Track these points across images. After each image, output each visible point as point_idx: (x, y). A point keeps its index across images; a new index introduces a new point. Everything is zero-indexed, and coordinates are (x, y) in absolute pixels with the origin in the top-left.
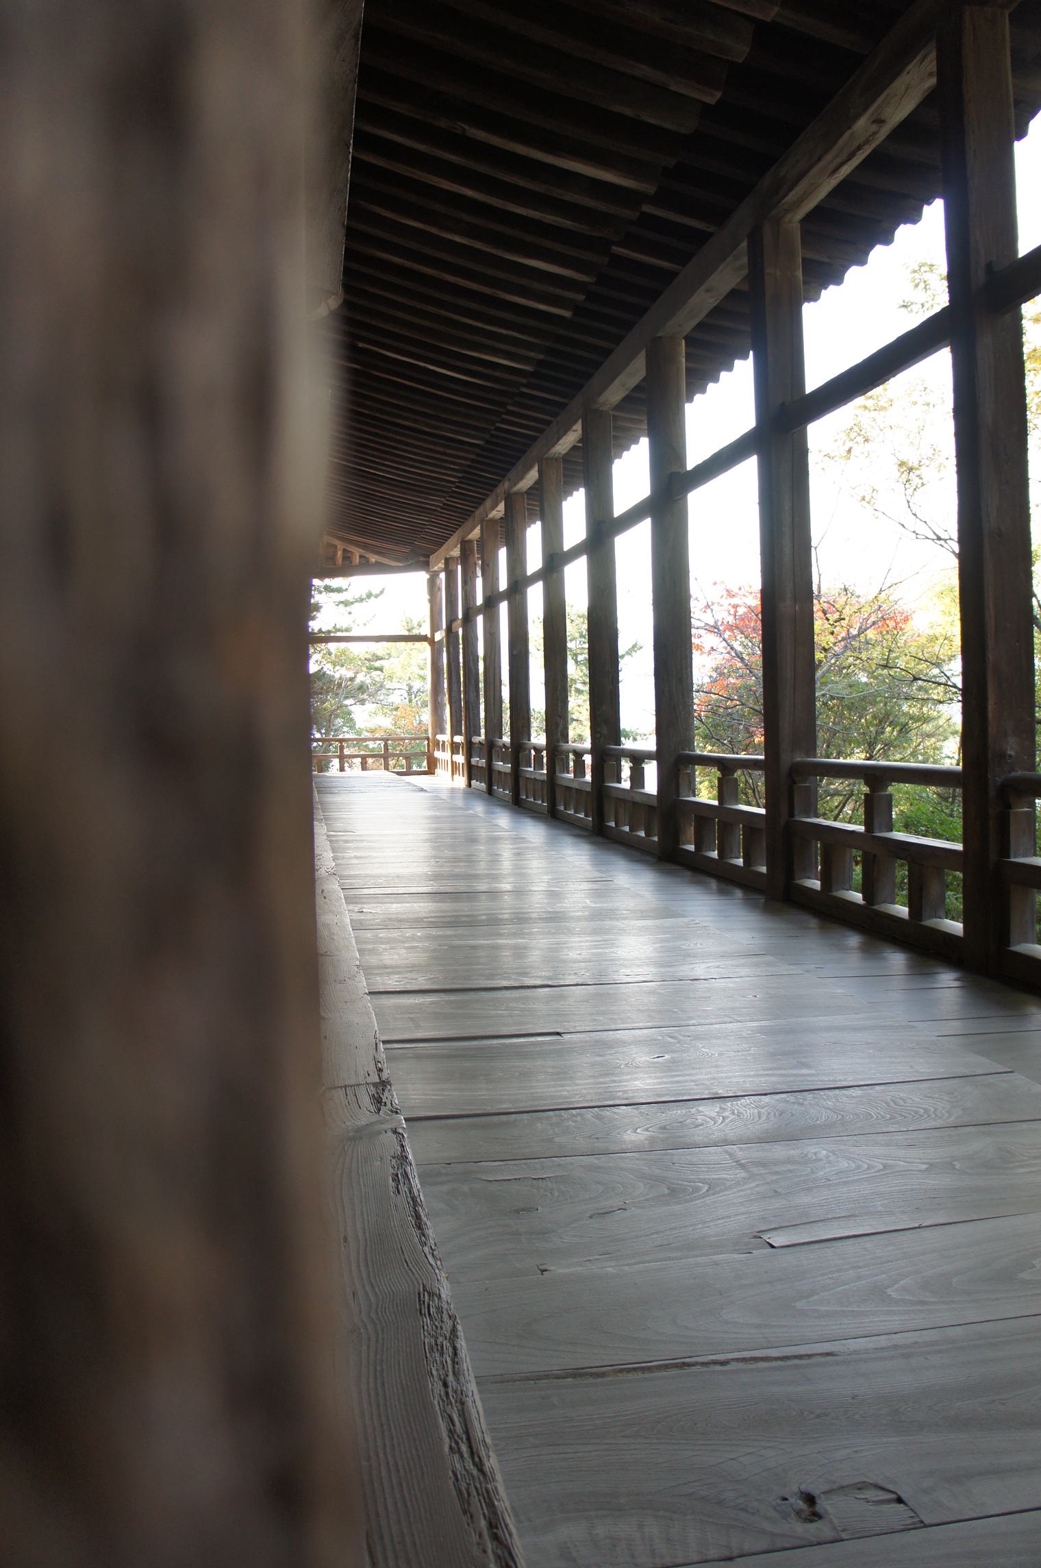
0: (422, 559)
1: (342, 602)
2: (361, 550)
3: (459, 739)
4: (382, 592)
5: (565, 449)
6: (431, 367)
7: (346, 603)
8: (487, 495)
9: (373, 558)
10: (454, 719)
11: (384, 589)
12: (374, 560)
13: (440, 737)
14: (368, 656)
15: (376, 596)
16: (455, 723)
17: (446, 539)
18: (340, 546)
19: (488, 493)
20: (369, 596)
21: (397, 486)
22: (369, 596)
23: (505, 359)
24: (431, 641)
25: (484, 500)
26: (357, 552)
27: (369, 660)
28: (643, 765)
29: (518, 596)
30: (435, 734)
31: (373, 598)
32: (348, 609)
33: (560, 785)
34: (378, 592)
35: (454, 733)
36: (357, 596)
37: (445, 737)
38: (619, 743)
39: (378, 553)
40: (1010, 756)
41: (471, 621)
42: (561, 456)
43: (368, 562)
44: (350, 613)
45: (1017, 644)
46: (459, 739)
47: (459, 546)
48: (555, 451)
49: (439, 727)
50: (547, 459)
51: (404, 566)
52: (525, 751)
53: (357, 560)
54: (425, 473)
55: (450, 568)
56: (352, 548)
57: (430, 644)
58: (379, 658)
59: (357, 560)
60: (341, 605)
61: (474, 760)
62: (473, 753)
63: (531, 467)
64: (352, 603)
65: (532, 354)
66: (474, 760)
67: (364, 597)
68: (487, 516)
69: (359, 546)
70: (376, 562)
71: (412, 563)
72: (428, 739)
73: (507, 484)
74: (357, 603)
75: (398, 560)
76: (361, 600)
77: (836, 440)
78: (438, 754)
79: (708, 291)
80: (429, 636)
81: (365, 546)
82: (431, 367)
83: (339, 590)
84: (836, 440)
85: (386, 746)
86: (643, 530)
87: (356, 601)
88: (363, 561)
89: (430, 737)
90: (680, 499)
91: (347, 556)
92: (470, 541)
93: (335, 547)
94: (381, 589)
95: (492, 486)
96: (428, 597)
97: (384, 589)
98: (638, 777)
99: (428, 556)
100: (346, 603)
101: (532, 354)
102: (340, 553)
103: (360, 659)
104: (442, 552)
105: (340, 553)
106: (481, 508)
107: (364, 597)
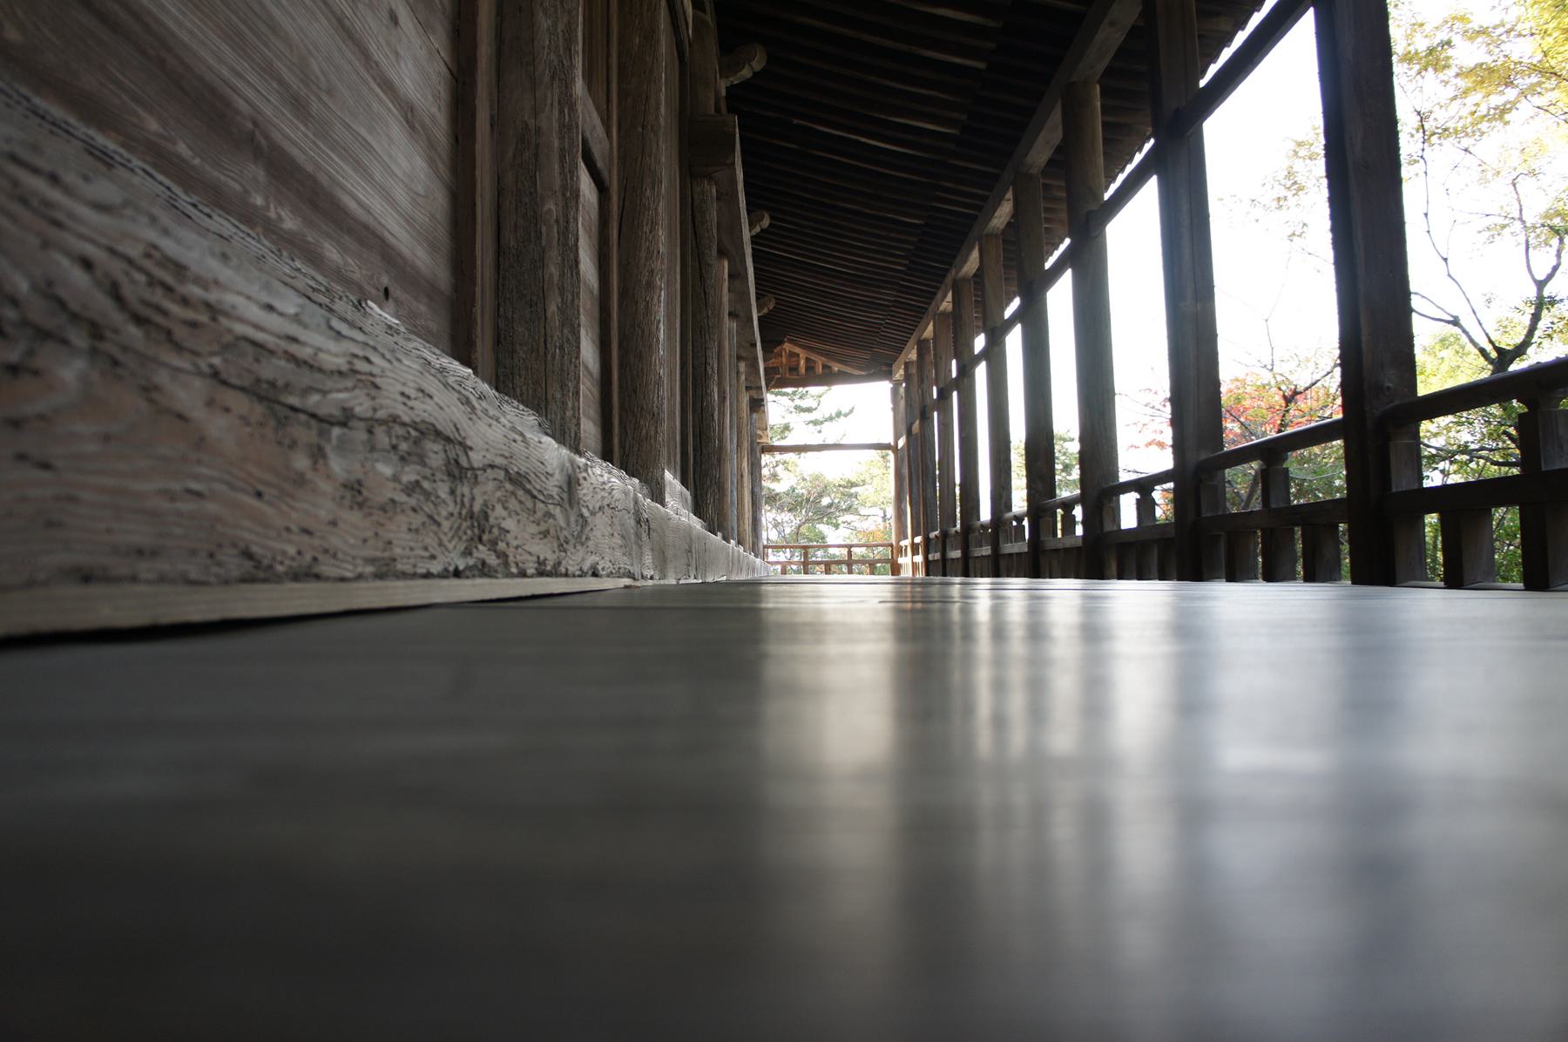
0: (884, 368)
1: (812, 422)
2: (823, 359)
3: (918, 540)
4: (851, 411)
5: (1002, 223)
6: (863, 140)
7: (815, 423)
8: (938, 288)
9: (836, 367)
10: (915, 521)
11: (853, 408)
12: (836, 369)
13: (903, 543)
14: (842, 483)
15: (846, 415)
16: (915, 525)
17: (905, 343)
18: (803, 354)
19: (938, 285)
20: (839, 414)
21: (846, 280)
22: (839, 414)
23: (932, 123)
24: (895, 449)
25: (935, 294)
26: (820, 361)
27: (844, 487)
28: (1073, 513)
29: (965, 380)
30: (898, 541)
31: (842, 417)
32: (818, 428)
33: (1004, 555)
34: (847, 411)
35: (914, 535)
36: (827, 416)
37: (906, 543)
38: (1053, 495)
39: (841, 362)
40: (1389, 388)
41: (929, 418)
42: (999, 233)
43: (831, 372)
44: (820, 432)
45: (1391, 275)
46: (918, 540)
47: (916, 347)
48: (993, 225)
49: (902, 534)
50: (986, 235)
51: (867, 375)
52: (974, 532)
53: (819, 369)
54: (863, 237)
55: (910, 372)
56: (813, 357)
57: (893, 452)
58: (853, 485)
59: (819, 369)
60: (811, 424)
61: (931, 557)
62: (930, 549)
63: (971, 249)
64: (822, 423)
65: (955, 115)
66: (931, 557)
67: (834, 415)
68: (938, 308)
69: (822, 355)
70: (839, 370)
71: (874, 373)
72: (891, 545)
73: (953, 272)
74: (826, 423)
75: (861, 369)
76: (831, 419)
77: (1264, 184)
78: (901, 560)
79: (1112, 24)
80: (892, 444)
81: (828, 355)
82: (863, 140)
83: (809, 410)
84: (1264, 184)
85: (850, 553)
86: (1066, 280)
87: (826, 421)
88: (827, 371)
89: (894, 544)
90: (1097, 237)
91: (810, 367)
92: (926, 341)
93: (798, 355)
94: (850, 408)
95: (940, 276)
96: (891, 406)
97: (853, 408)
98: (1069, 522)
99: (891, 366)
100: (815, 423)
101: (955, 115)
102: (802, 362)
103: (835, 485)
104: (902, 359)
105: (802, 362)
106: (934, 303)
107: (834, 415)
